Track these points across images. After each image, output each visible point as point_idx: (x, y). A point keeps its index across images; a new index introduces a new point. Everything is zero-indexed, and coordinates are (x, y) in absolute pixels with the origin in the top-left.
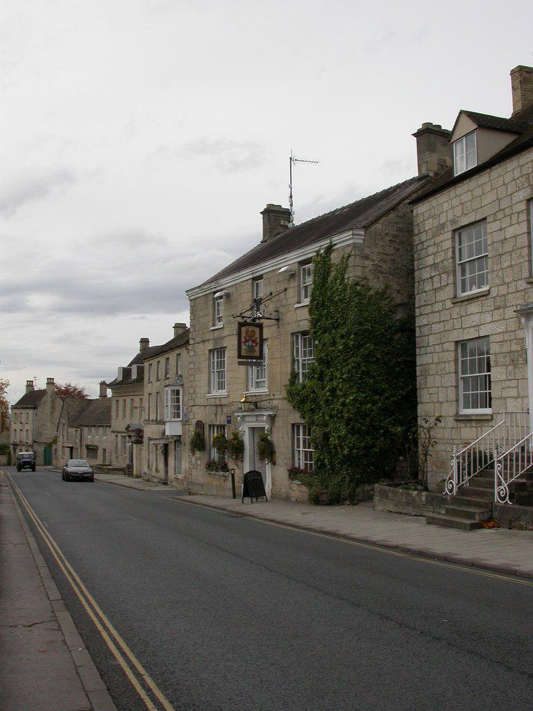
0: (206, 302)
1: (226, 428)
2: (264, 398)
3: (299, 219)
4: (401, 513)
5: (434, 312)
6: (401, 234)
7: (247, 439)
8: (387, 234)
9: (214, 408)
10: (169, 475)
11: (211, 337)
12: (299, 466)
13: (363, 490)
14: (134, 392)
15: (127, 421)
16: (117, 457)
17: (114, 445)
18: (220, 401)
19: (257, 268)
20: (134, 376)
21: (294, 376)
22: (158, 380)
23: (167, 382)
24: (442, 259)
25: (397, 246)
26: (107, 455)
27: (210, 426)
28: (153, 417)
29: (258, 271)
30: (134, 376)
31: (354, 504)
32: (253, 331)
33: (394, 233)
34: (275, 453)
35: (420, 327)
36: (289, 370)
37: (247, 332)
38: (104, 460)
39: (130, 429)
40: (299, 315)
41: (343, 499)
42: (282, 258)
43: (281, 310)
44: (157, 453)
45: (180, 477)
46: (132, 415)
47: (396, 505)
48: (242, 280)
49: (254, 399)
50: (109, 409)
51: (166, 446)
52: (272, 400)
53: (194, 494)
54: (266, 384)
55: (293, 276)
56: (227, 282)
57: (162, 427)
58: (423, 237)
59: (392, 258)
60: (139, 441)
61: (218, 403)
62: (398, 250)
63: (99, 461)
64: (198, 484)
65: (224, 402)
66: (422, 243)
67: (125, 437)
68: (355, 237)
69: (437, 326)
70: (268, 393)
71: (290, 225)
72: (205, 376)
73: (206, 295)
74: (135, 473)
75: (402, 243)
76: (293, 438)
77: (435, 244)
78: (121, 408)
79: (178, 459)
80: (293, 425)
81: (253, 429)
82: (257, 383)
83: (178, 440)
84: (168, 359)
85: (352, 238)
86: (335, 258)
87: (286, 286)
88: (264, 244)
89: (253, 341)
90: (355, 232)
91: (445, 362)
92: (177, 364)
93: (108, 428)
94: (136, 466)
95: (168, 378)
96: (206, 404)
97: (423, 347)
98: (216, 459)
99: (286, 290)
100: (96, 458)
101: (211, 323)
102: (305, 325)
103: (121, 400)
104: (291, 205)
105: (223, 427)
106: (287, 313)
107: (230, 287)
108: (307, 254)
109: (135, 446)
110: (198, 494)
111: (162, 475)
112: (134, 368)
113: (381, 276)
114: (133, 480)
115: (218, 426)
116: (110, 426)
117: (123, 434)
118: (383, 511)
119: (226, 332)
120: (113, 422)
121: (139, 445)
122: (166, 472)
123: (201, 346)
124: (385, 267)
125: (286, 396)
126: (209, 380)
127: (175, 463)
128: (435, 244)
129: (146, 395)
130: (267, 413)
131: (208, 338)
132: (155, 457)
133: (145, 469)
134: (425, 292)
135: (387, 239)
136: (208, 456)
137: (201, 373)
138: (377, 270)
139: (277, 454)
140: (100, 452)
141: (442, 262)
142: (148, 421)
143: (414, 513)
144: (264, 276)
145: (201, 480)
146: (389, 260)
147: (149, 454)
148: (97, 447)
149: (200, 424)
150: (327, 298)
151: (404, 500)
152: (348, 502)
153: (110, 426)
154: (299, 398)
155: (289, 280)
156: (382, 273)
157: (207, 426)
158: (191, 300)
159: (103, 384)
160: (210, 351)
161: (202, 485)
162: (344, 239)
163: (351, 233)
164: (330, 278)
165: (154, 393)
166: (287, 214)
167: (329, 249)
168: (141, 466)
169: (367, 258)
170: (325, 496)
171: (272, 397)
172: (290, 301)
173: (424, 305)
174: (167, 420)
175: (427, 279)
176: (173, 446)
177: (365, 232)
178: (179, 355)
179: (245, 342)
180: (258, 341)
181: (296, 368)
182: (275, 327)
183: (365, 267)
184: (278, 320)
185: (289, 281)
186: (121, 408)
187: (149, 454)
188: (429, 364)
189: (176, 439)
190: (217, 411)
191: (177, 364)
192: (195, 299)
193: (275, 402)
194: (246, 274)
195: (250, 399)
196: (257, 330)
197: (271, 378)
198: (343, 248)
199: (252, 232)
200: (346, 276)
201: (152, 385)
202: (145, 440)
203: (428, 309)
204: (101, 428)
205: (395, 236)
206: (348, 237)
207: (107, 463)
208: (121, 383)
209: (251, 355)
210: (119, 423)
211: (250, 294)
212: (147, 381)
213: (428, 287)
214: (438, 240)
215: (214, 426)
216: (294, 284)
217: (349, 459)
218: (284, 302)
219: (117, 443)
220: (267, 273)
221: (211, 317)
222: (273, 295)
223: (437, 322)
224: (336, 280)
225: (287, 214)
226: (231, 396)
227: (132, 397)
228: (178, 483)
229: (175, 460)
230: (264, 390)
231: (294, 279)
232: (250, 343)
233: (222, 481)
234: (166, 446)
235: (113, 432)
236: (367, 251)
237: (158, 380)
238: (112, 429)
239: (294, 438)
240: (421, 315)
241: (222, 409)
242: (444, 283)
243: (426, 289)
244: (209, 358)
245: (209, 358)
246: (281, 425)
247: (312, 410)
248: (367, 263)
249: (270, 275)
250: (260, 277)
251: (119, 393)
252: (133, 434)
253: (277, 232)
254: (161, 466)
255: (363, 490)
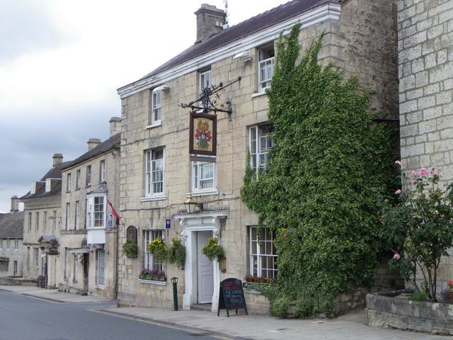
0: (141, 100)
1: (163, 233)
2: (212, 199)
3: (233, 20)
4: (411, 330)
5: (427, 96)
6: (376, 14)
7: (189, 245)
8: (362, 12)
9: (149, 213)
10: (89, 285)
11: (147, 137)
12: (255, 274)
13: (340, 301)
14: (47, 205)
15: (41, 234)
16: (28, 269)
17: (26, 257)
18: (157, 204)
19: (204, 57)
20: (48, 189)
21: (250, 173)
22: (78, 189)
23: (89, 190)
24: (439, 34)
25: (373, 27)
26: (18, 266)
27: (144, 231)
28: (71, 226)
29: (205, 62)
30: (48, 189)
31: (331, 318)
32: (206, 124)
33: (370, 12)
34: (225, 259)
35: (406, 114)
36: (244, 167)
37: (200, 123)
38: (15, 272)
39: (43, 241)
40: (256, 107)
41: (318, 312)
42: (235, 44)
43: (234, 101)
44: (75, 264)
45: (102, 287)
46: (45, 227)
47: (404, 320)
48: (185, 73)
49: (199, 201)
50: (21, 223)
51: (86, 256)
52: (221, 200)
53: (124, 306)
54: (215, 184)
55: (248, 63)
56: (165, 77)
57: (82, 237)
58: (411, 12)
59: (367, 39)
60: (54, 252)
61: (154, 206)
62: (373, 31)
63: (10, 273)
64: (128, 295)
65: (161, 205)
66: (410, 19)
67: (37, 249)
68: (331, 12)
69: (432, 111)
70: (217, 193)
71: (225, 27)
72: (139, 178)
73: (141, 92)
74: (49, 284)
75: (377, 23)
76: (248, 243)
77: (428, 18)
78: (33, 221)
79: (101, 269)
80: (248, 227)
81: (196, 234)
82: (202, 183)
83: (101, 249)
84: (89, 167)
85: (328, 14)
86: (304, 41)
87: (240, 75)
88: (198, 45)
89: (206, 135)
90: (331, 7)
91: (443, 152)
92: (100, 171)
93: (20, 241)
94: (51, 277)
95: (90, 186)
96: (139, 207)
97: (411, 136)
98: (151, 268)
99: (240, 79)
100: (7, 270)
101: (147, 122)
102: (263, 117)
103: (34, 213)
104: (226, 6)
105: (158, 233)
106: (240, 104)
107: (169, 81)
108: (267, 37)
109: (50, 257)
110: (128, 306)
111: (80, 285)
112: (48, 182)
113: (357, 58)
114: (48, 291)
115: (153, 231)
116: (22, 239)
117: (35, 246)
118: (382, 327)
119: (165, 130)
120: (25, 235)
121: (54, 256)
122: (86, 282)
123: (135, 147)
124: (360, 49)
125: (240, 196)
126: (144, 182)
127: (96, 273)
128: (428, 18)
129: (64, 205)
130: (215, 215)
131: (143, 137)
132: (73, 268)
133: (62, 281)
134: (414, 74)
135: (363, 18)
136: (141, 264)
137: (134, 175)
138: (353, 51)
139: (228, 260)
140: (11, 264)
141: (440, 37)
142: (65, 232)
143: (435, 331)
144: (213, 66)
145: (132, 290)
146: (365, 42)
147: (66, 265)
148: (8, 259)
149: (132, 231)
150: (296, 86)
151: (417, 313)
152: (323, 315)
153: (22, 239)
154: (254, 195)
155: (244, 67)
156: (358, 55)
157: (141, 231)
158: (122, 99)
159: (14, 199)
160: (145, 151)
161: (134, 296)
162: (316, 16)
163: (326, 7)
164: (297, 63)
165: (73, 202)
166: (222, 15)
167: (296, 30)
168: (55, 277)
169: (342, 37)
170: (294, 308)
171: (221, 197)
172: (245, 91)
173: (413, 89)
174: (90, 228)
175: (417, 59)
176: (94, 255)
177: (341, 8)
178: (103, 161)
179: (197, 136)
180: (211, 135)
181: (251, 163)
182: (227, 121)
183: (341, 47)
184: (230, 112)
185: (245, 68)
186: (33, 221)
187: (66, 265)
188: (419, 156)
189: (98, 248)
190: (152, 215)
191: (100, 171)
192: (127, 97)
193: (226, 203)
194: (191, 65)
195: (194, 200)
196: (210, 123)
197: (221, 175)
198: (314, 26)
199: (187, 37)
200: (319, 57)
201: (71, 195)
202: (61, 249)
203: (419, 93)
204: (13, 241)
205: (370, 16)
206: (324, 13)
207: (18, 274)
208: (34, 196)
209: (203, 148)
210: (31, 236)
211: (195, 87)
212: (66, 190)
213: (417, 67)
214: (432, 13)
215: (148, 232)
216: (250, 71)
217: (327, 266)
218: (238, 92)
219: (29, 255)
220: (214, 63)
221: (147, 115)
222: (224, 86)
223: (431, 107)
224: (306, 62)
225: (222, 15)
226: (170, 198)
227: (45, 210)
228: (99, 294)
229: (97, 269)
230: (212, 190)
231: (251, 66)
232: (203, 137)
233: (158, 292)
234: (86, 256)
235: (25, 244)
236: (343, 29)
237: (78, 189)
238: (24, 241)
239: (249, 242)
240: (407, 100)
241: (159, 212)
242: (441, 61)
243: (415, 70)
244: (144, 160)
245: (144, 160)
246: (233, 228)
247: (275, 209)
248: (344, 43)
249: (220, 65)
250: (208, 68)
251: (30, 206)
252: (46, 246)
253: (212, 33)
254: (80, 276)
255: (340, 301)
